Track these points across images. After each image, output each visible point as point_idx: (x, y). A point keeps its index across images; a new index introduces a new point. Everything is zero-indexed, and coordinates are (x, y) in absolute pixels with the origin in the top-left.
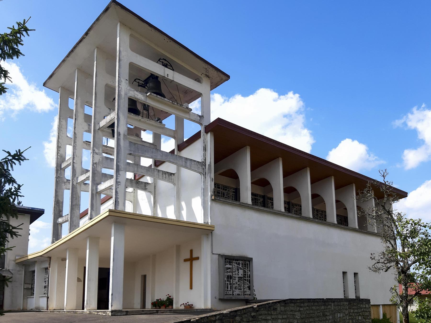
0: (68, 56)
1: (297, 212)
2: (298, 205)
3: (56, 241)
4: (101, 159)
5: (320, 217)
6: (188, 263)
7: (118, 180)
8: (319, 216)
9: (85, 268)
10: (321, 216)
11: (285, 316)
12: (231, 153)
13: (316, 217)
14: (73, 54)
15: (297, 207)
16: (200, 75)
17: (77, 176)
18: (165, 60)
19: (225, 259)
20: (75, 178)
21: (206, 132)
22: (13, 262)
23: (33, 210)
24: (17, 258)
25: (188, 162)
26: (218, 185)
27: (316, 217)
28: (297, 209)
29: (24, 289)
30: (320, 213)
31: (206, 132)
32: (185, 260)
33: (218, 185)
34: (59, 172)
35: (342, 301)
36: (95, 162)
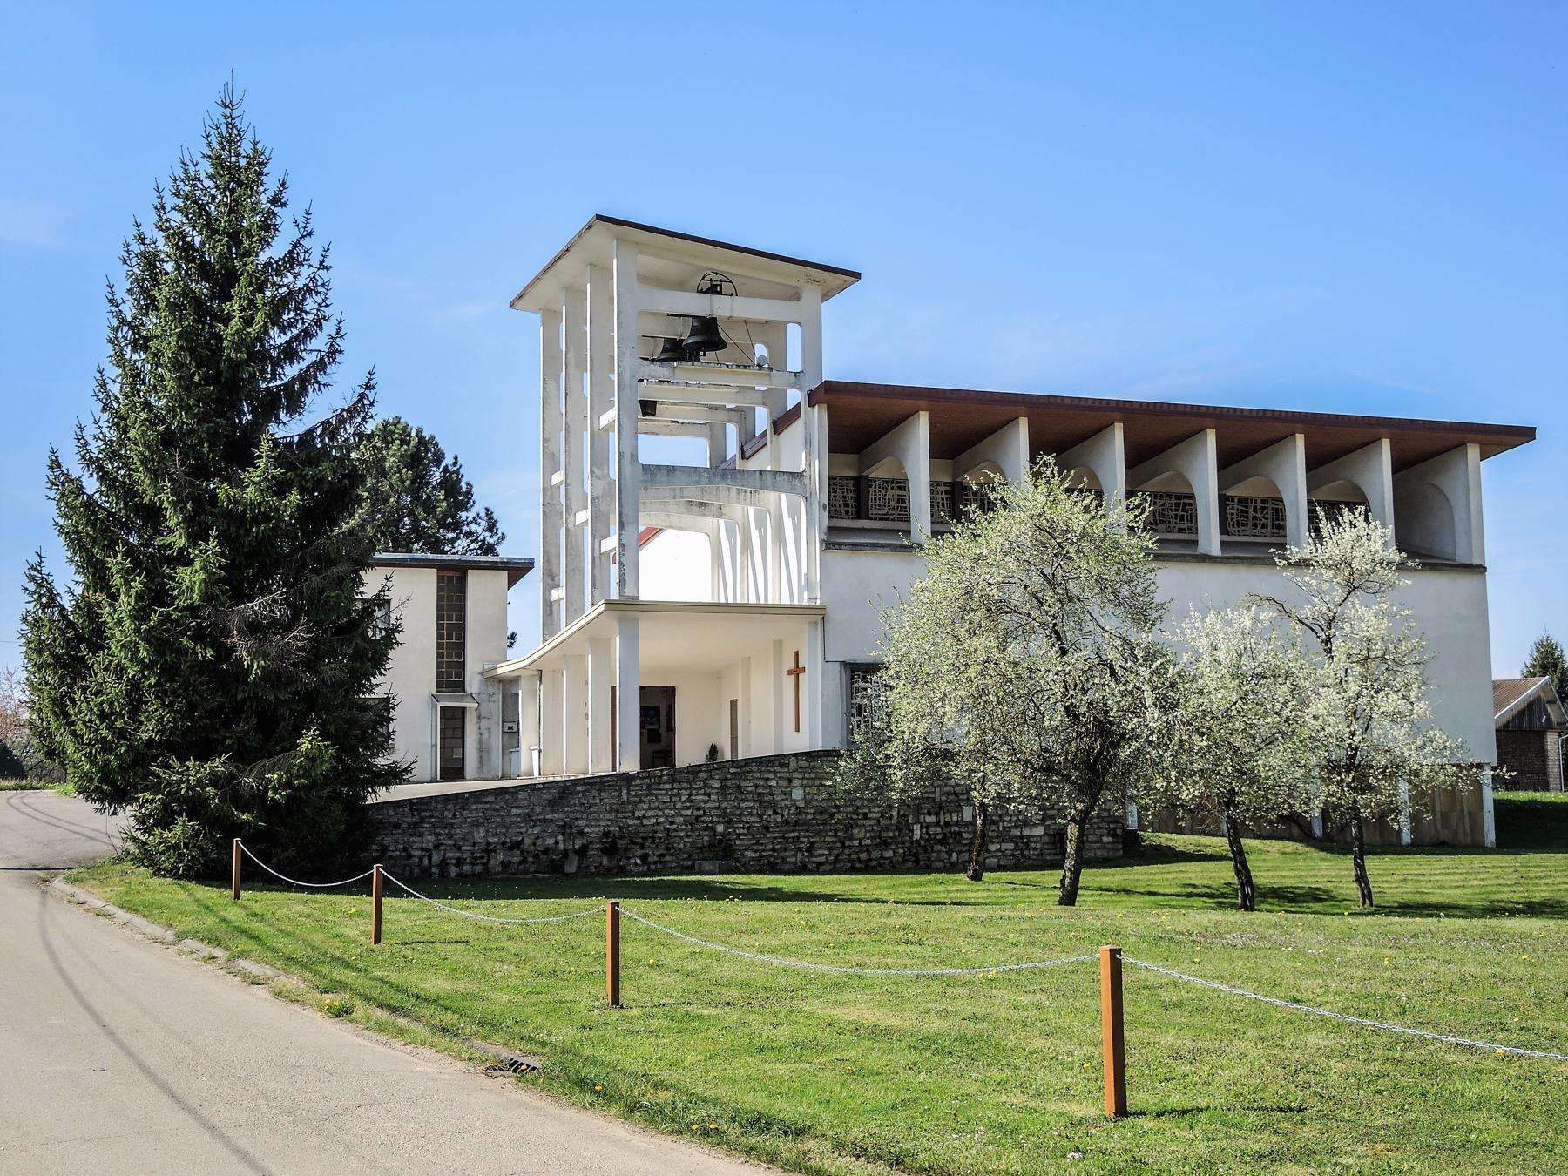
0: (545, 272)
1: (1163, 515)
2: (1168, 495)
3: (550, 636)
4: (606, 487)
5: (1255, 518)
6: (793, 677)
7: (623, 542)
8: (1252, 513)
9: (613, 689)
10: (1258, 515)
11: (813, 776)
12: (897, 424)
13: (1238, 521)
14: (550, 272)
15: (1162, 502)
16: (794, 283)
17: (574, 511)
18: (716, 274)
19: (853, 672)
20: (572, 516)
21: (811, 404)
22: (480, 677)
23: (510, 563)
24: (486, 667)
25: (769, 480)
26: (898, 483)
27: (1238, 521)
28: (1163, 505)
29: (503, 732)
30: (1255, 507)
31: (811, 404)
32: (789, 673)
33: (901, 483)
34: (549, 493)
35: (819, 757)
36: (595, 495)
